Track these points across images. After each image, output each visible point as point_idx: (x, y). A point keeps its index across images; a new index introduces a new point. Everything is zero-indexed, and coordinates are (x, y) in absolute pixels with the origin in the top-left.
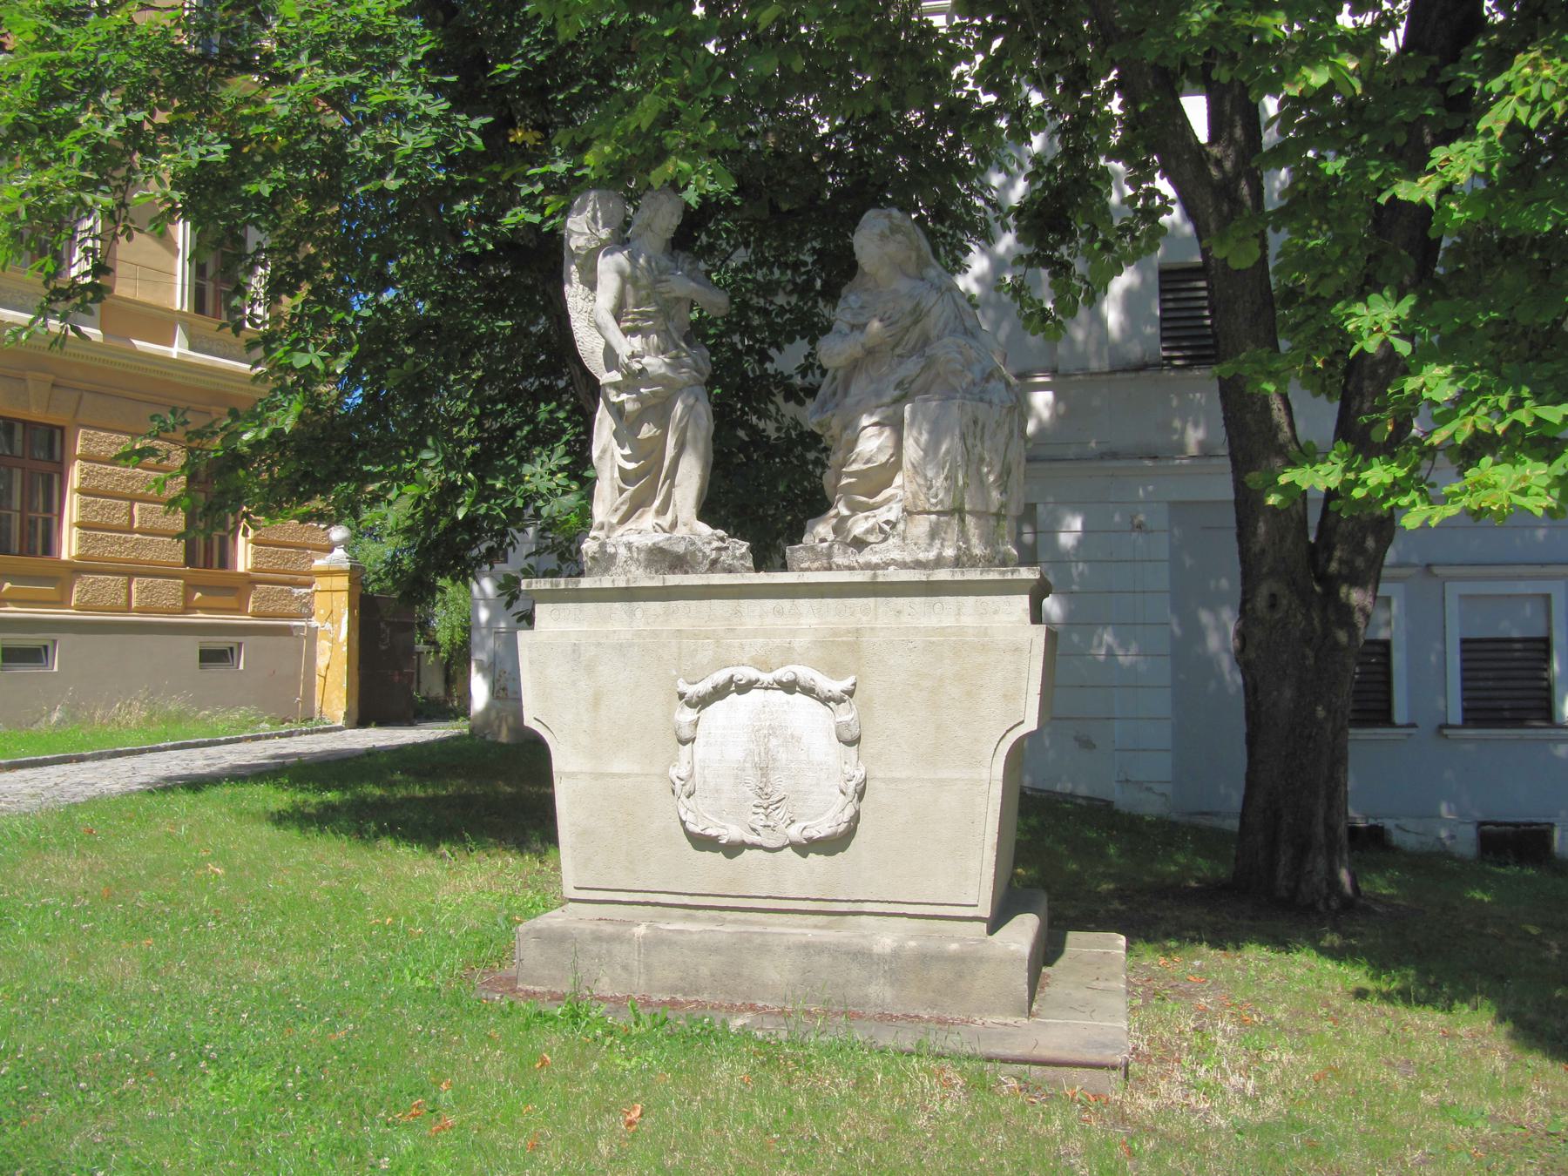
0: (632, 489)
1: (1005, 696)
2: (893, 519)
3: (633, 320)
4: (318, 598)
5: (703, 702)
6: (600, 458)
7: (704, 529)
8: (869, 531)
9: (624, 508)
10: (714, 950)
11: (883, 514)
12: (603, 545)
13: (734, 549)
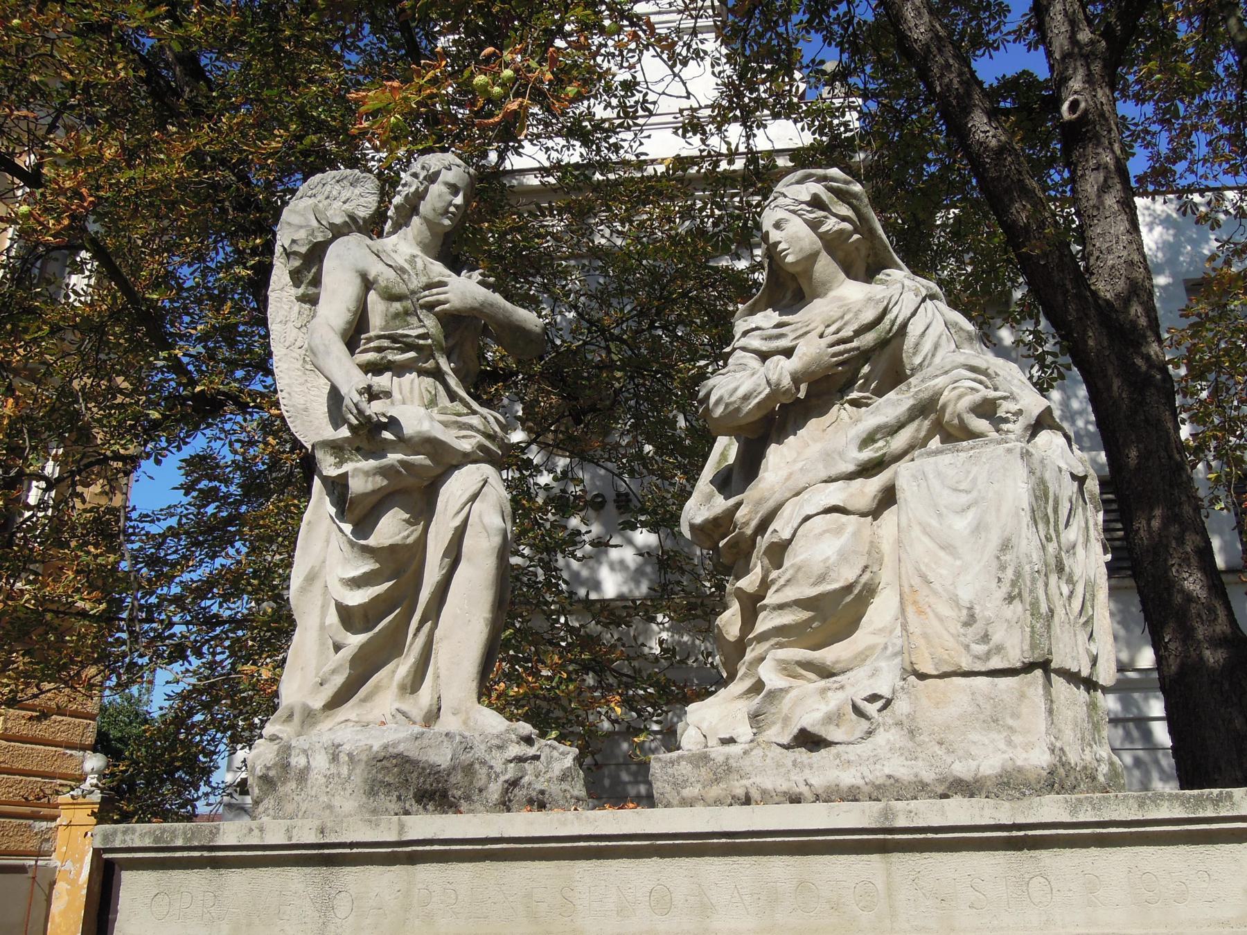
0: (361, 638)
2: (885, 691)
4: (61, 834)
6: (303, 590)
7: (492, 721)
8: (834, 718)
11: (858, 685)
12: (286, 750)
13: (550, 760)
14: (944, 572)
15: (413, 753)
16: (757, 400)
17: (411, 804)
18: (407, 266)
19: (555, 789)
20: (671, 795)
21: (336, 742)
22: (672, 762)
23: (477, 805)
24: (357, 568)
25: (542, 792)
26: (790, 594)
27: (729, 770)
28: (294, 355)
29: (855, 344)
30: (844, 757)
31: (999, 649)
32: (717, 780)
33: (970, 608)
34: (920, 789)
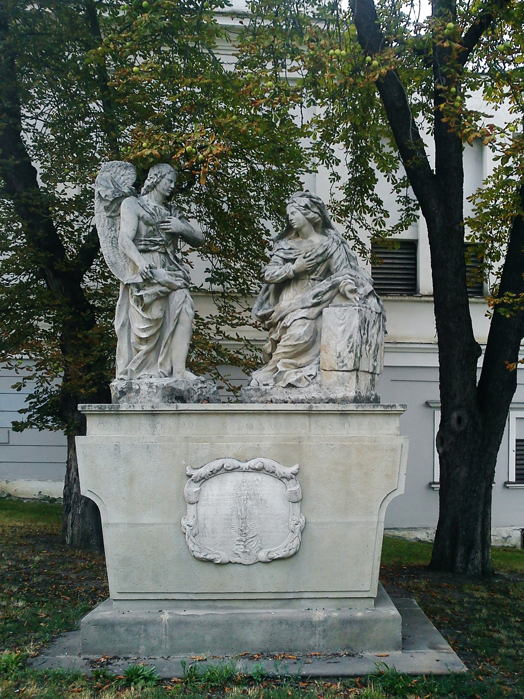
1: (386, 475)
2: (314, 374)
3: (145, 245)
5: (204, 479)
7: (191, 376)
8: (299, 380)
9: (140, 361)
10: (215, 625)
14: (333, 342)
15: (175, 386)
16: (281, 277)
17: (174, 400)
18: (153, 212)
19: (212, 397)
20: (247, 400)
21: (151, 382)
22: (248, 390)
23: (191, 401)
24: (144, 325)
25: (208, 398)
26: (288, 343)
27: (266, 393)
28: (108, 240)
29: (315, 261)
30: (301, 391)
31: (346, 365)
32: (262, 396)
33: (340, 353)
34: (321, 401)
